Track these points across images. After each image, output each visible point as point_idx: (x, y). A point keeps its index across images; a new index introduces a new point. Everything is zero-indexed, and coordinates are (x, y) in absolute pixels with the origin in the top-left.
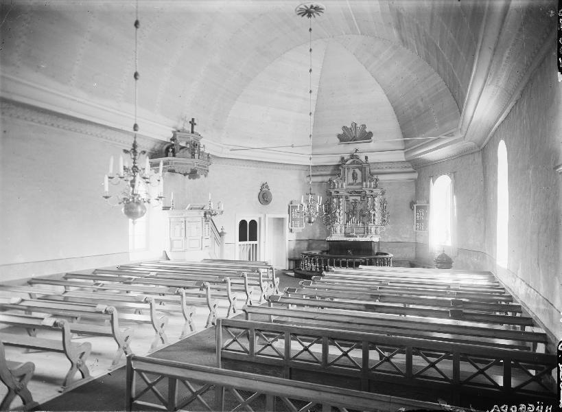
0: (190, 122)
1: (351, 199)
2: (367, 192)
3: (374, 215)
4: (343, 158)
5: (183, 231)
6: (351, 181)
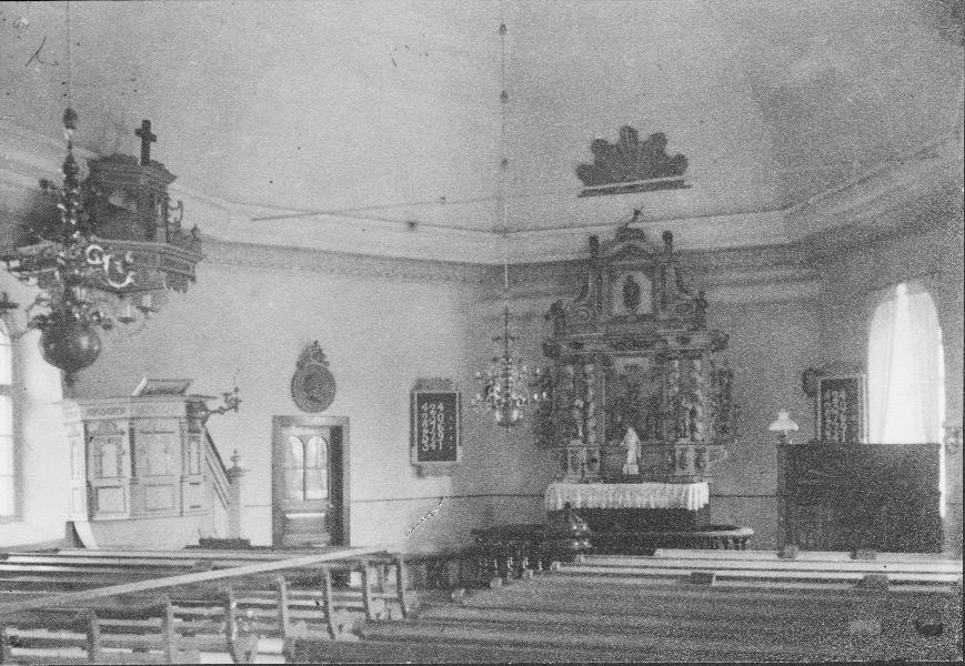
0: (138, 132)
1: (620, 365)
2: (672, 343)
3: (693, 413)
4: (593, 240)
5: (127, 460)
6: (619, 308)
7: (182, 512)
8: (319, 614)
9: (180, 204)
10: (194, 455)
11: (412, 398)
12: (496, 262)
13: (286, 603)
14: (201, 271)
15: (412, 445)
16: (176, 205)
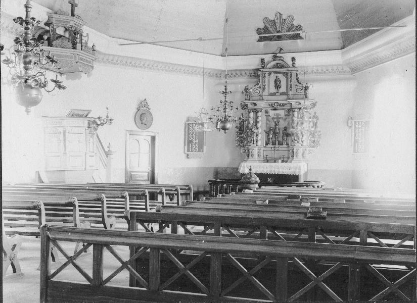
6: (273, 90)
7: (86, 168)
8: (101, 219)
9: (87, 34)
10: (91, 142)
11: (186, 125)
12: (223, 69)
13: (105, 206)
14: (96, 65)
15: (185, 145)
16: (86, 35)
